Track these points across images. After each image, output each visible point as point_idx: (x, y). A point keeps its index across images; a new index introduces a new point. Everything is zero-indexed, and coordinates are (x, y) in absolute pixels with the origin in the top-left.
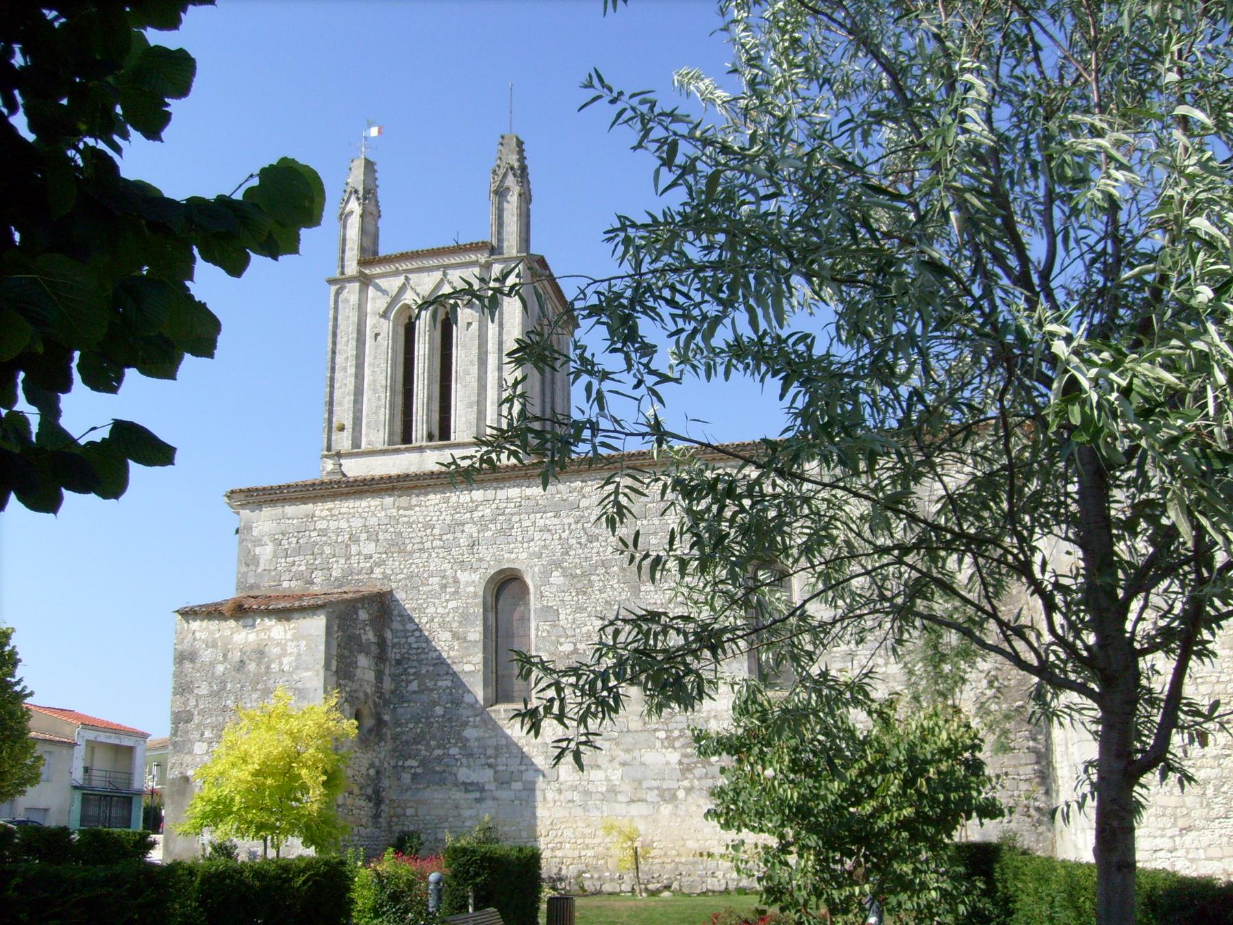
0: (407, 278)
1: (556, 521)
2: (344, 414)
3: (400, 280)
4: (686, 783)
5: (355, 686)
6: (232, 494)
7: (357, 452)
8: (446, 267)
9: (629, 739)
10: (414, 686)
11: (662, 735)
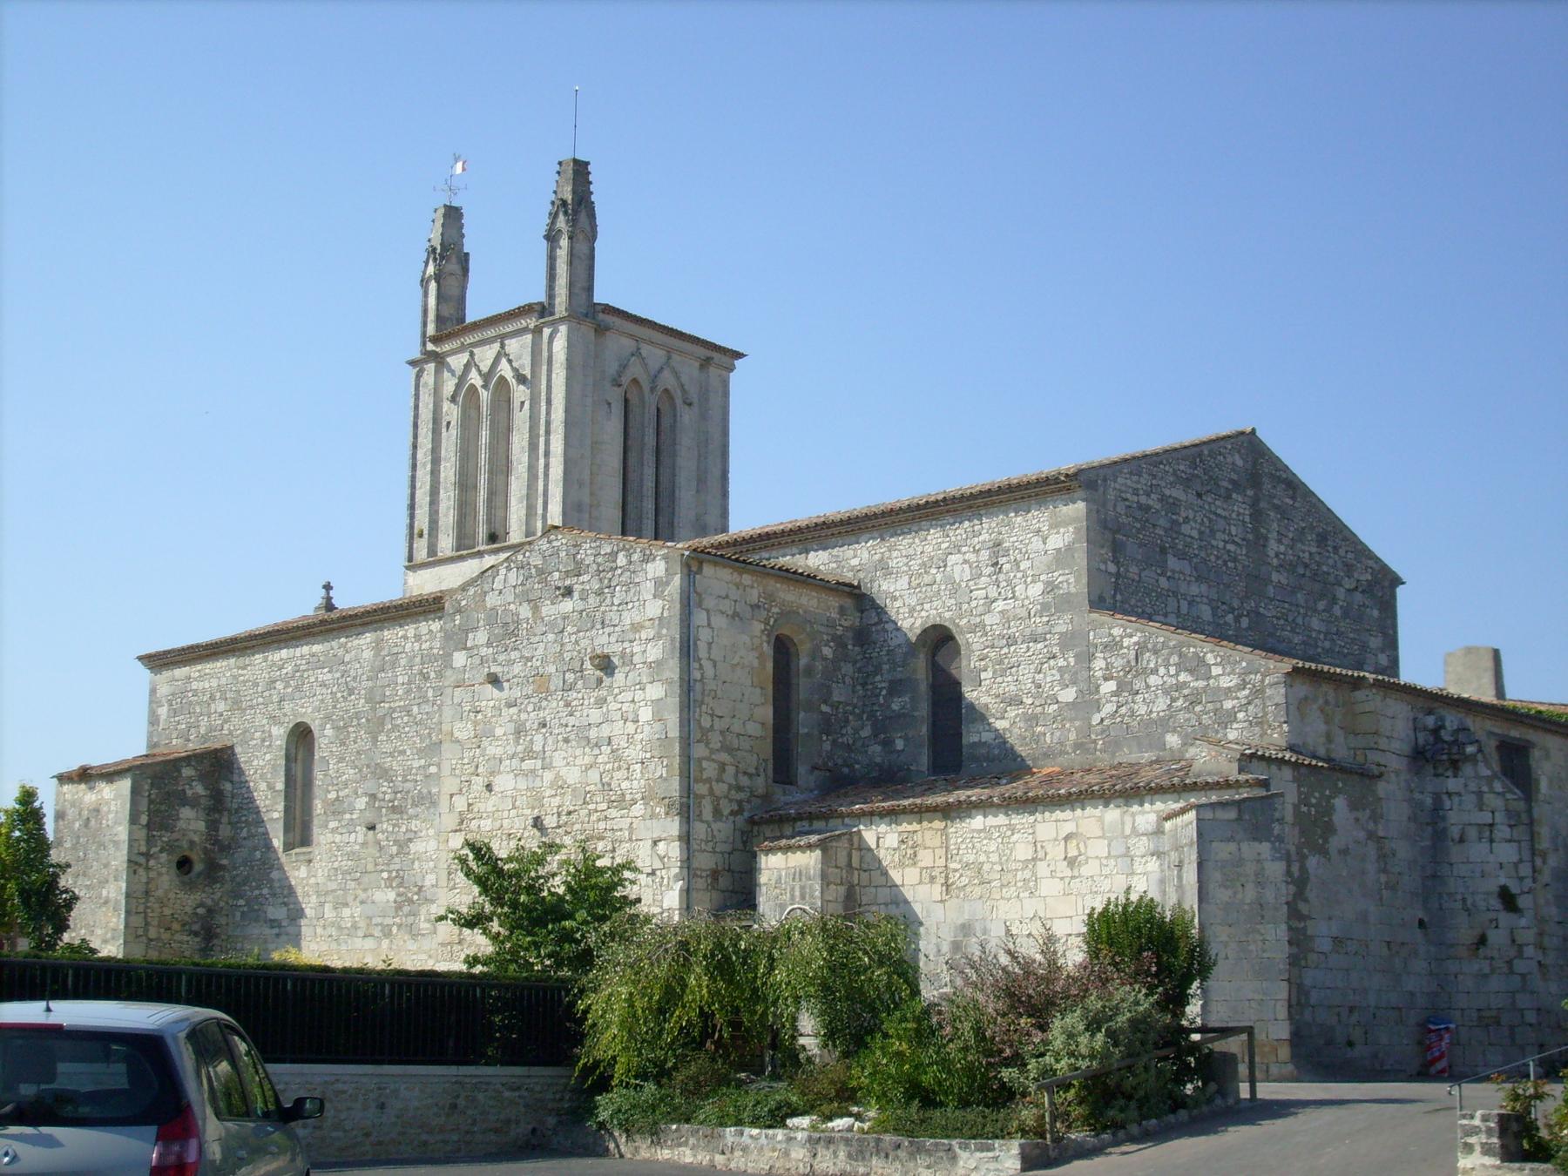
0: (472, 354)
1: (329, 676)
2: (422, 521)
3: (465, 357)
4: (397, 920)
5: (175, 836)
6: (140, 658)
7: (434, 561)
8: (502, 338)
9: (366, 879)
10: (244, 833)
11: (385, 875)
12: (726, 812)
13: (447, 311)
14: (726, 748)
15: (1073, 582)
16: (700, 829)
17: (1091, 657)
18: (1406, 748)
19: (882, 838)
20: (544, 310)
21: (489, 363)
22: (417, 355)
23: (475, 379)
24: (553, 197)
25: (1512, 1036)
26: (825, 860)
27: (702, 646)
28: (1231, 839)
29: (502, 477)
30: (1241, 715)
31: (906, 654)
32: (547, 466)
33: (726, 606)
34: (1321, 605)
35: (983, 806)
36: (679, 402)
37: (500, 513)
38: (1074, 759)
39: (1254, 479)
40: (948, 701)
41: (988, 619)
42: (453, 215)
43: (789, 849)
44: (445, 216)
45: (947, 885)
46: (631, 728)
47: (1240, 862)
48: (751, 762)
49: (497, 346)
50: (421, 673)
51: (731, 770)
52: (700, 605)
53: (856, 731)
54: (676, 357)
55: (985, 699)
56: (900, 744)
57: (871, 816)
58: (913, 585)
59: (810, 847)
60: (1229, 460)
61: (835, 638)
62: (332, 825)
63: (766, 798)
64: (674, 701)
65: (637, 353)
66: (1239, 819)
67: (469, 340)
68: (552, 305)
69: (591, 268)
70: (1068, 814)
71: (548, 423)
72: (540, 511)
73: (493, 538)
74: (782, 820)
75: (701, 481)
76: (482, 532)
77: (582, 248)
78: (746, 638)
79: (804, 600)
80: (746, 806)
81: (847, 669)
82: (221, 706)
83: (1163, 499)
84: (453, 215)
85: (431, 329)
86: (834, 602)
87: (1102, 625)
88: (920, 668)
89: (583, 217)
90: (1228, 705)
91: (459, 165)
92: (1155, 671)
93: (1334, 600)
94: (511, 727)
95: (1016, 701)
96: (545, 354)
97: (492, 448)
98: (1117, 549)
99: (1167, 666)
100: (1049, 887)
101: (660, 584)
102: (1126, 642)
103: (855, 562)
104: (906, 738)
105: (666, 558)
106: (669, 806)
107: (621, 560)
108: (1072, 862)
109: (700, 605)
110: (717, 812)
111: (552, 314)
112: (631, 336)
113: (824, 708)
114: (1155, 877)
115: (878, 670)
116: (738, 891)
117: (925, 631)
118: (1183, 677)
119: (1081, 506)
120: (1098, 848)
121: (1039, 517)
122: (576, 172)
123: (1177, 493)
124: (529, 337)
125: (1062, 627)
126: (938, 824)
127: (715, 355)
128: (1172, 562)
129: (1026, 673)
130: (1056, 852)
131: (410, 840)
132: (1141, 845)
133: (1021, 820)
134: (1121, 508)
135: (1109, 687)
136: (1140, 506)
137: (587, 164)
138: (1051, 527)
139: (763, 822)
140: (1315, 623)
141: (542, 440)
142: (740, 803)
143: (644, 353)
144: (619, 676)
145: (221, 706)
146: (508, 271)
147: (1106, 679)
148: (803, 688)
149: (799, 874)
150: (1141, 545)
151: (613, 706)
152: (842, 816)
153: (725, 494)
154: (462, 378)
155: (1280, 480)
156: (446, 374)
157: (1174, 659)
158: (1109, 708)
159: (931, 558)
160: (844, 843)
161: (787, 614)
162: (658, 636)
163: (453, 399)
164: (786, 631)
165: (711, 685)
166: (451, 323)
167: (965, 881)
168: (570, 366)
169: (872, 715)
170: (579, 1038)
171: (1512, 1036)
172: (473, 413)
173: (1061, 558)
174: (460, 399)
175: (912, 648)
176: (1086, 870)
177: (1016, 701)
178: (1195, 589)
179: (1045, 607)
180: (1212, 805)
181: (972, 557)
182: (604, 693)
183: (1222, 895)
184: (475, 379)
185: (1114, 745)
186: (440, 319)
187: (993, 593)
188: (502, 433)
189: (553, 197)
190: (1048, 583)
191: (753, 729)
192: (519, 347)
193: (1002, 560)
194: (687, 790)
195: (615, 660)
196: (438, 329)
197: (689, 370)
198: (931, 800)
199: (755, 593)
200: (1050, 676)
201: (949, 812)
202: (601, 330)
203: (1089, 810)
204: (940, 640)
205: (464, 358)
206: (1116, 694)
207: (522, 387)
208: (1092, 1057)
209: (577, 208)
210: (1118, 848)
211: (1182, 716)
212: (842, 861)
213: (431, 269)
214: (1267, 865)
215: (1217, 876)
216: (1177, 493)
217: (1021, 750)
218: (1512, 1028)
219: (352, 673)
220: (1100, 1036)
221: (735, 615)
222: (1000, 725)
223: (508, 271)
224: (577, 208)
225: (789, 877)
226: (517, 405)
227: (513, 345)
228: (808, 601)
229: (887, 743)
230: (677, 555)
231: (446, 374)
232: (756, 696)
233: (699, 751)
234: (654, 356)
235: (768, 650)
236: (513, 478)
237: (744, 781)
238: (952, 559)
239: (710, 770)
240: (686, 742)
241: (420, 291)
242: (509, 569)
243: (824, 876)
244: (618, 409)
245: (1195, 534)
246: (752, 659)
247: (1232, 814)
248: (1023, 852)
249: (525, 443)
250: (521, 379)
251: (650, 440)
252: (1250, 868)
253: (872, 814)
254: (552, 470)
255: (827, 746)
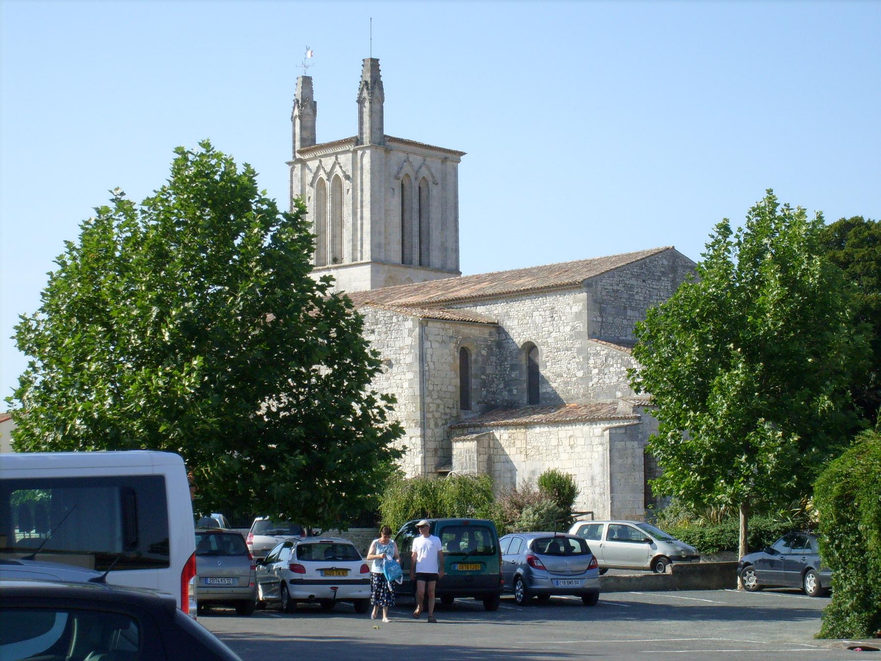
0: (320, 161)
8: (336, 154)
12: (440, 424)
13: (306, 135)
14: (439, 397)
15: (582, 326)
16: (429, 432)
17: (589, 359)
19: (502, 435)
20: (358, 141)
22: (291, 159)
23: (322, 175)
24: (360, 79)
26: (479, 445)
27: (429, 356)
28: (623, 440)
29: (338, 228)
31: (517, 354)
32: (362, 224)
33: (439, 338)
35: (540, 423)
36: (430, 183)
37: (338, 247)
38: (582, 400)
39: (673, 269)
40: (533, 370)
41: (549, 340)
42: (307, 81)
43: (464, 440)
44: (303, 82)
45: (527, 455)
46: (400, 390)
47: (626, 449)
48: (450, 403)
51: (442, 407)
52: (427, 339)
53: (498, 385)
54: (428, 159)
55: (548, 374)
56: (515, 392)
57: (498, 426)
58: (522, 322)
59: (472, 440)
60: (660, 262)
61: (487, 346)
63: (458, 417)
64: (417, 380)
65: (407, 160)
66: (626, 433)
67: (319, 154)
68: (362, 138)
69: (382, 118)
70: (570, 428)
71: (362, 202)
72: (359, 248)
73: (335, 260)
74: (464, 427)
75: (444, 224)
76: (329, 257)
77: (376, 107)
78: (447, 351)
79: (473, 331)
80: (449, 421)
81: (493, 359)
83: (625, 285)
84: (307, 81)
85: (298, 147)
86: (487, 331)
87: (593, 345)
88: (523, 360)
89: (377, 91)
91: (309, 53)
92: (612, 366)
95: (560, 375)
96: (359, 165)
97: (333, 213)
98: (602, 311)
99: (617, 364)
100: (564, 456)
101: (411, 331)
102: (602, 353)
103: (496, 312)
104: (517, 389)
105: (412, 320)
106: (416, 423)
107: (394, 320)
108: (572, 447)
109: (427, 339)
110: (436, 425)
111: (362, 143)
112: (404, 152)
113: (483, 377)
114: (601, 453)
115: (506, 359)
116: (444, 458)
117: (525, 344)
119: (584, 295)
120: (581, 441)
121: (569, 298)
122: (372, 66)
123: (633, 282)
124: (351, 155)
125: (577, 345)
126: (523, 430)
127: (448, 155)
128: (629, 313)
129: (564, 364)
130: (566, 442)
132: (596, 441)
133: (553, 429)
134: (604, 293)
135: (595, 371)
136: (613, 290)
137: (378, 60)
139: (456, 428)
141: (359, 210)
142: (446, 420)
143: (411, 159)
144: (395, 368)
146: (338, 119)
148: (474, 369)
149: (468, 451)
150: (614, 307)
151: (393, 381)
152: (486, 426)
153: (457, 230)
154: (316, 174)
155: (688, 267)
156: (307, 171)
157: (620, 361)
158: (595, 380)
160: (486, 438)
161: (466, 338)
162: (410, 352)
163: (311, 185)
164: (465, 345)
165: (433, 372)
166: (308, 143)
167: (533, 453)
168: (372, 172)
169: (504, 379)
170: (380, 518)
172: (322, 192)
173: (577, 316)
174: (315, 185)
175: (520, 351)
176: (577, 450)
177: (560, 375)
179: (571, 336)
180: (615, 428)
181: (543, 313)
182: (388, 375)
183: (619, 461)
184: (322, 175)
185: (597, 395)
186: (303, 140)
187: (551, 330)
188: (338, 205)
189: (360, 79)
190: (572, 326)
191: (451, 389)
192: (345, 159)
194: (423, 416)
195: (393, 362)
196: (302, 146)
197: (435, 165)
198: (519, 420)
199: (451, 331)
200: (573, 366)
201: (527, 426)
202: (388, 150)
203: (578, 426)
204: (531, 348)
205: (316, 163)
206: (598, 374)
207: (347, 181)
208: (534, 521)
209: (373, 86)
210: (588, 442)
211: (622, 385)
212: (486, 445)
213: (296, 112)
215: (617, 454)
216: (633, 282)
217: (562, 396)
220: (537, 516)
221: (443, 341)
222: (554, 385)
223: (338, 119)
224: (373, 86)
225: (465, 453)
226: (345, 191)
227: (342, 158)
228: (474, 331)
229: (510, 391)
230: (417, 319)
231: (307, 171)
232: (452, 374)
233: (428, 400)
234: (416, 160)
235: (457, 355)
236: (344, 230)
237: (448, 411)
238: (535, 314)
239: (433, 407)
240: (422, 396)
241: (291, 123)
243: (478, 451)
244: (398, 191)
245: (642, 298)
246: (450, 359)
247: (623, 431)
248: (554, 442)
249: (351, 212)
250: (347, 177)
251: (416, 206)
252: (630, 451)
253: (498, 425)
254: (364, 227)
255: (484, 393)
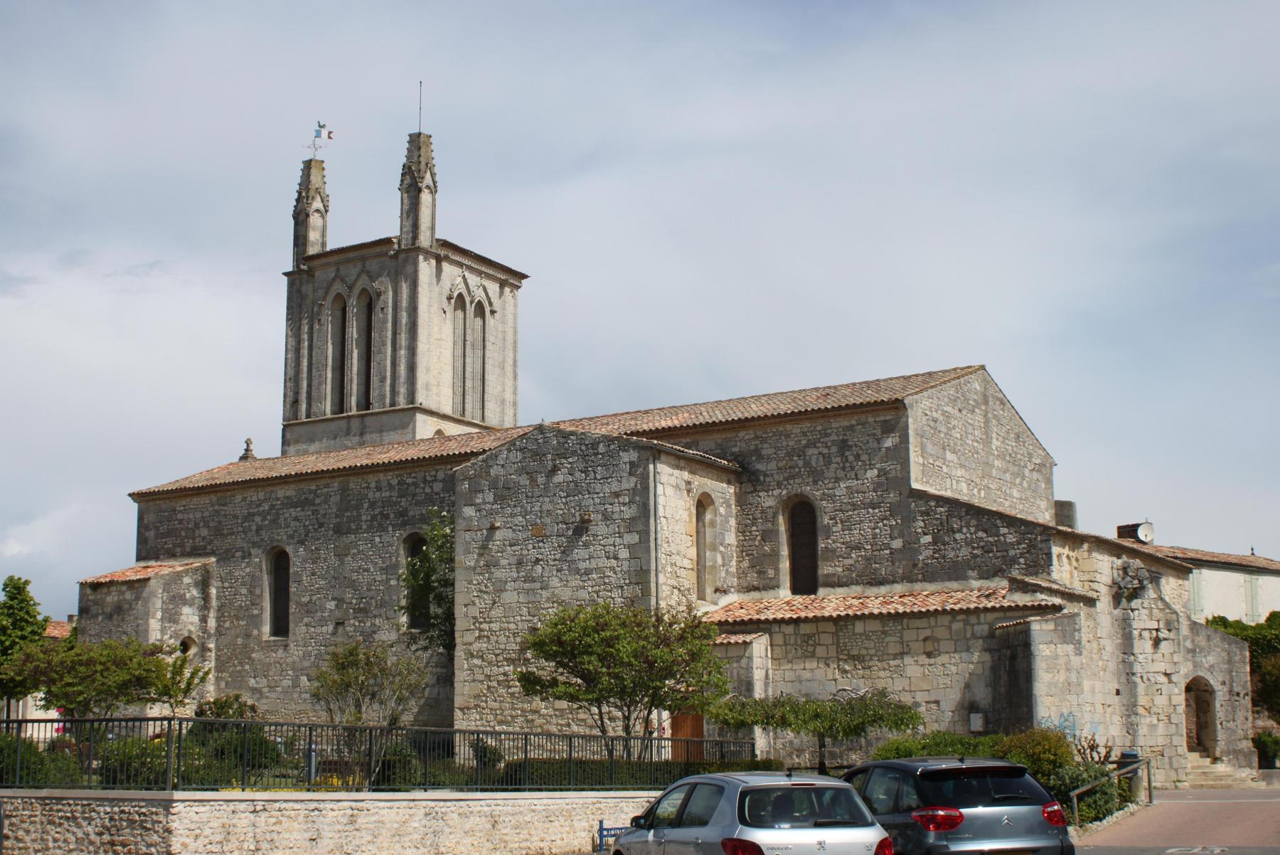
5: (179, 627)
18: (1109, 581)
21: (353, 278)
25: (1171, 764)
30: (1022, 560)
34: (1018, 481)
47: (1056, 657)
49: (359, 265)
50: (381, 513)
62: (306, 620)
82: (204, 532)
90: (1012, 553)
92: (960, 531)
93: (1023, 478)
94: (514, 560)
118: (980, 534)
128: (949, 456)
131: (374, 632)
138: (883, 433)
140: (1015, 493)
145: (204, 532)
147: (925, 534)
159: (794, 449)
171: (1171, 764)
178: (959, 472)
181: (825, 451)
193: (847, 453)
214: (1072, 658)
218: (1170, 758)
219: (323, 512)
238: (810, 451)
242: (509, 451)
252: (1062, 661)
